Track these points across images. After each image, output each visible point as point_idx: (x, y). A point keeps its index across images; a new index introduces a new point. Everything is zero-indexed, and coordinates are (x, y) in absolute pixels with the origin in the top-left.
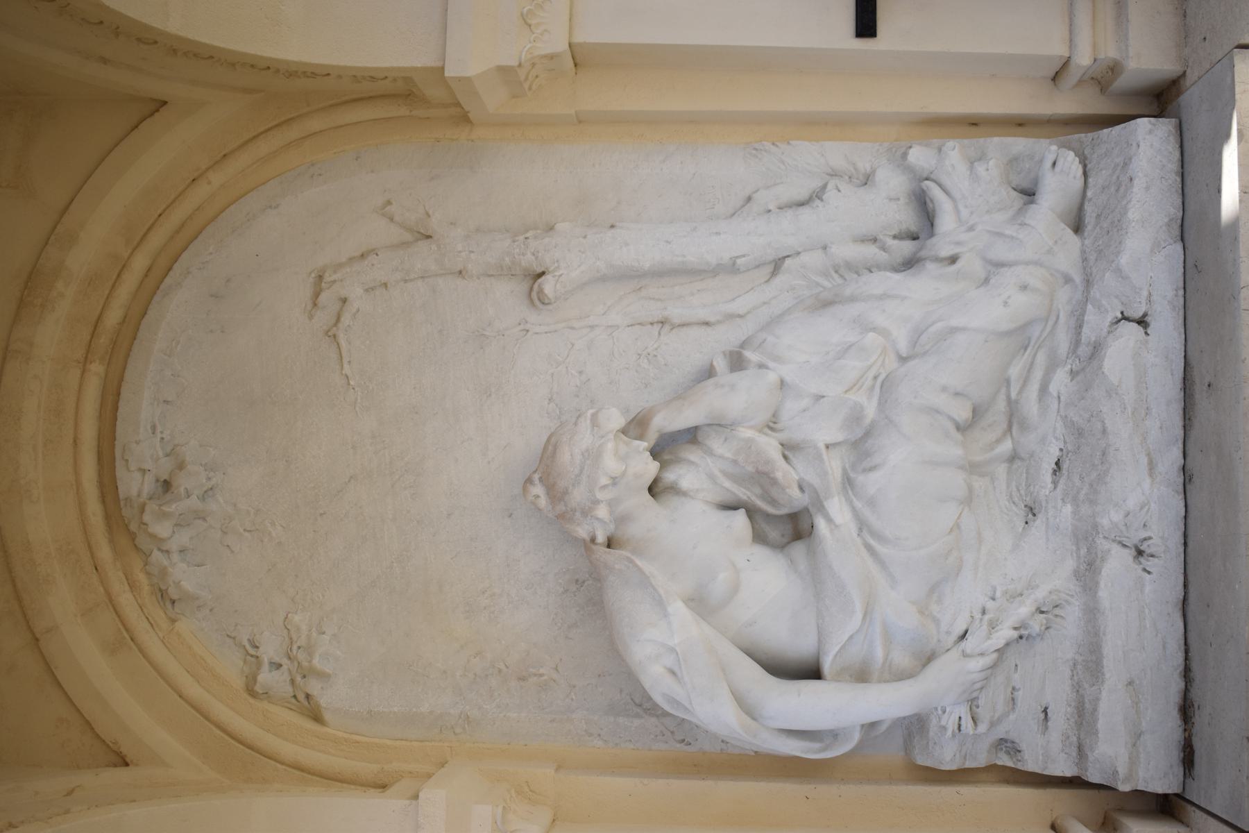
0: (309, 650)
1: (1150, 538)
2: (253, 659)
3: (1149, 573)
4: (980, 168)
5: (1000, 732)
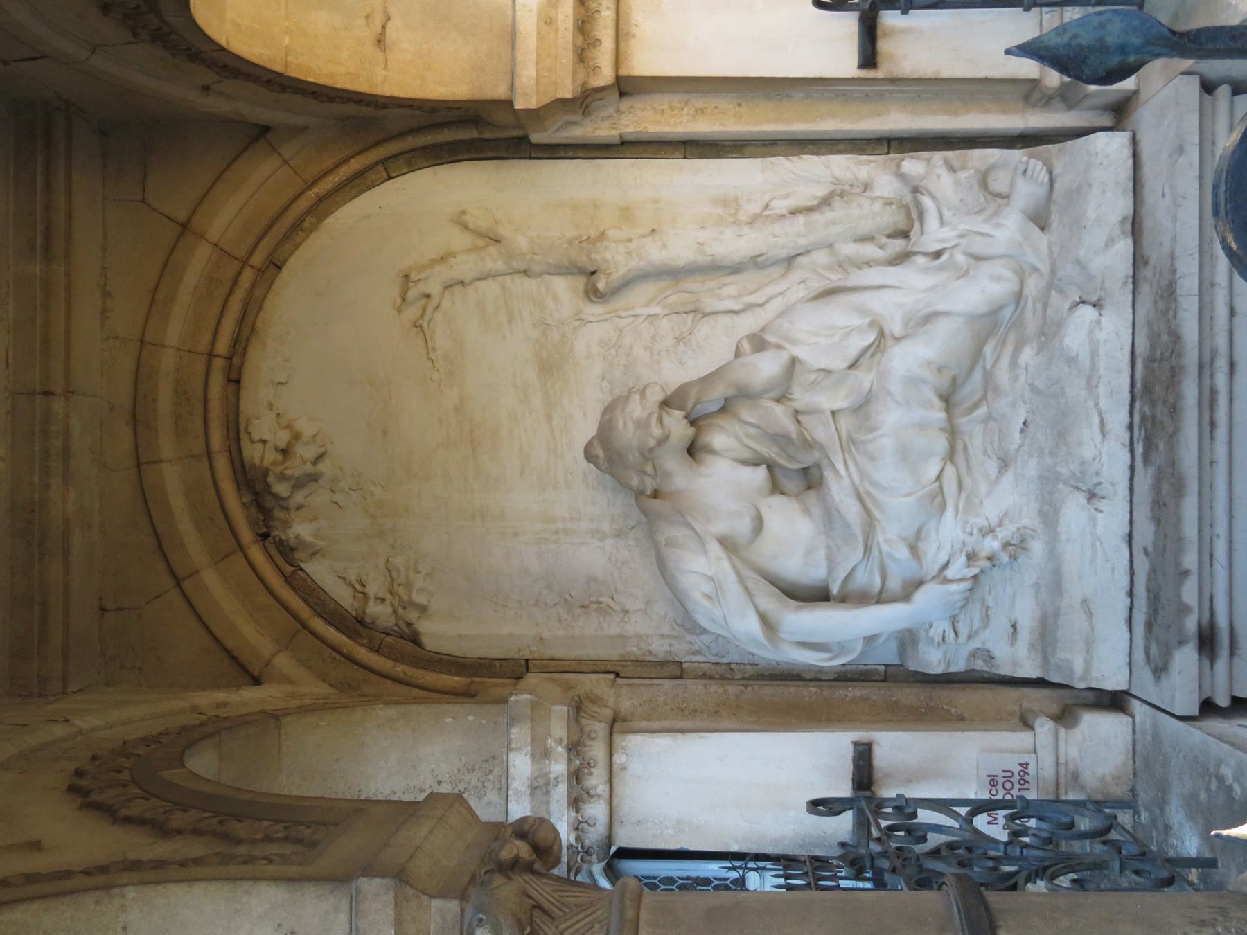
2: (361, 595)
3: (1101, 511)
5: (976, 643)
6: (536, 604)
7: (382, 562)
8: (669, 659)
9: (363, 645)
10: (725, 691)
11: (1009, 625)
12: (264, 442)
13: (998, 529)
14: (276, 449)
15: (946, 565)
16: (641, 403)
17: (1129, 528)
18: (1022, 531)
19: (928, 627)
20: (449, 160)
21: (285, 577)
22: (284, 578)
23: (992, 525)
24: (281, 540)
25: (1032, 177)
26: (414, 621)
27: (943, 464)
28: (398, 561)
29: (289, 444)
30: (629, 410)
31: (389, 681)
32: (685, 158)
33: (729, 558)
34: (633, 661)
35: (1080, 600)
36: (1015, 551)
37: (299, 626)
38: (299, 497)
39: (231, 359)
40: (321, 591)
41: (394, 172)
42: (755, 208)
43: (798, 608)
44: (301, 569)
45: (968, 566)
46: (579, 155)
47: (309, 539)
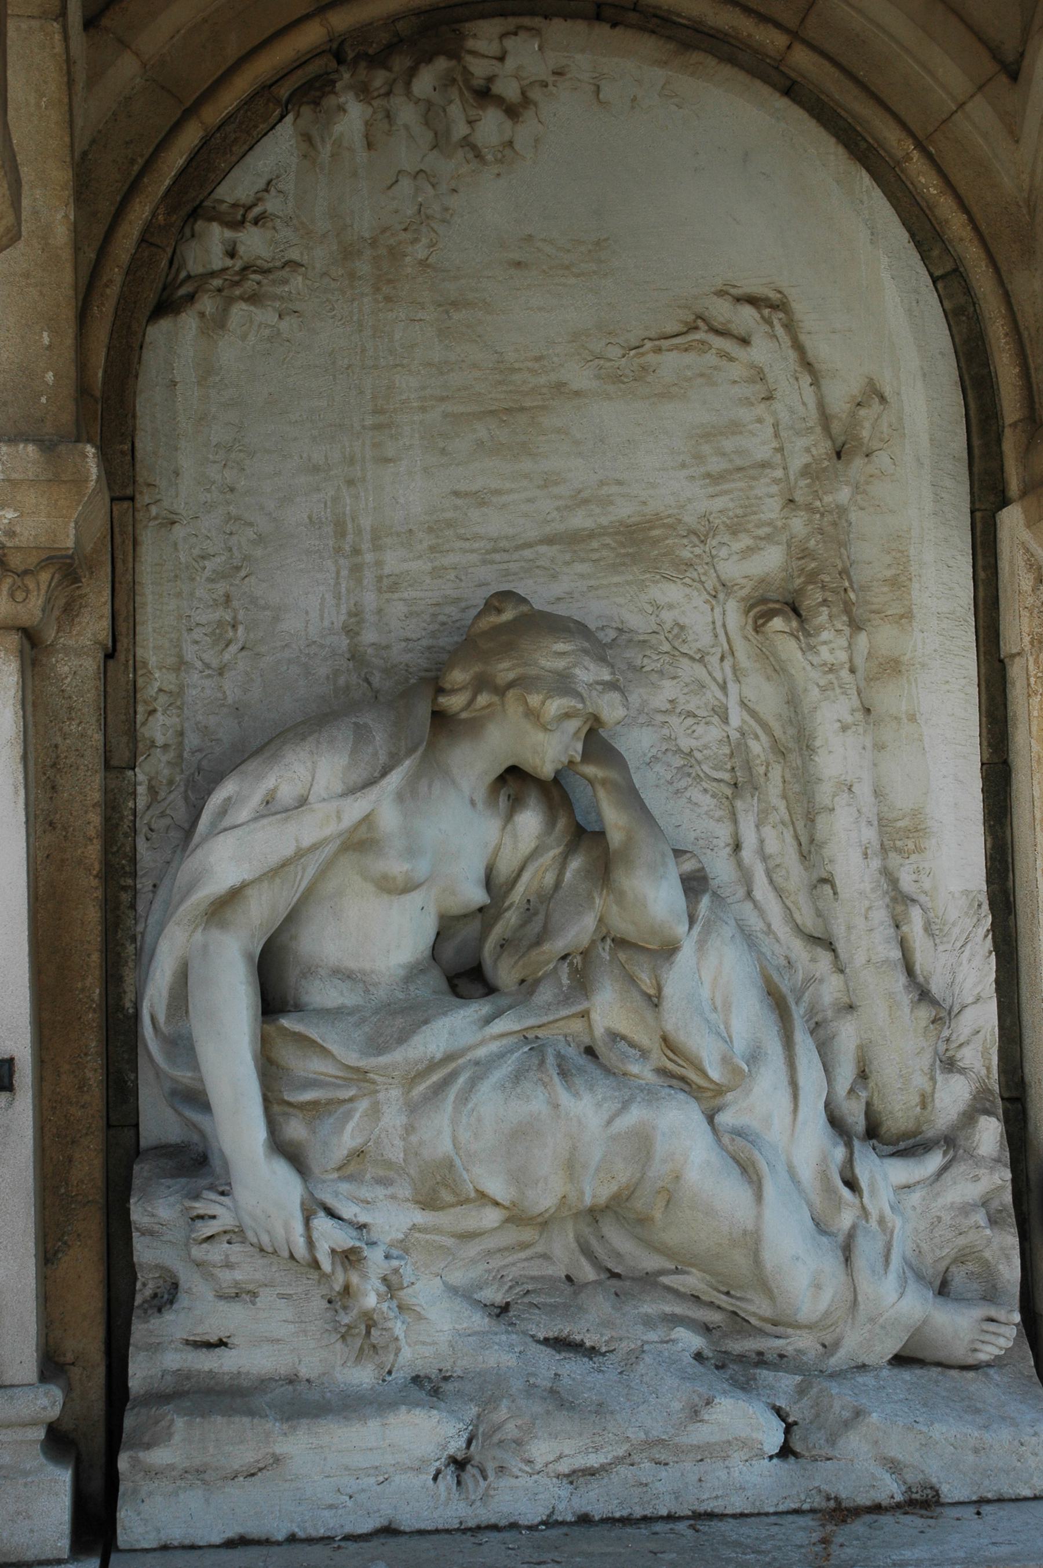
0: (253, 299)
1: (485, 1478)
2: (239, 217)
3: (435, 1478)
4: (980, 1218)
5: (188, 1277)
6: (229, 518)
7: (294, 255)
8: (140, 745)
9: (154, 214)
10: (91, 840)
11: (223, 1334)
12: (501, 59)
13: (394, 1304)
14: (491, 79)
15: (331, 1213)
16: (598, 683)
17: (408, 1529)
18: (392, 1346)
19: (221, 1189)
20: (966, 377)
21: (271, 86)
22: (269, 83)
23: (401, 1293)
24: (333, 82)
25: (983, 1331)
26: (198, 306)
27: (507, 1203)
28: (298, 282)
29: (499, 101)
30: (587, 661)
31: (93, 256)
32: (982, 764)
33: (340, 835)
34: (135, 682)
35: (278, 1452)
36: (358, 1334)
37: (188, 104)
38: (407, 114)
39: (634, 10)
40: (246, 147)
41: (945, 287)
42: (906, 882)
43: (249, 956)
44: (282, 117)
45: (333, 1251)
46: (981, 589)
47: (338, 129)
